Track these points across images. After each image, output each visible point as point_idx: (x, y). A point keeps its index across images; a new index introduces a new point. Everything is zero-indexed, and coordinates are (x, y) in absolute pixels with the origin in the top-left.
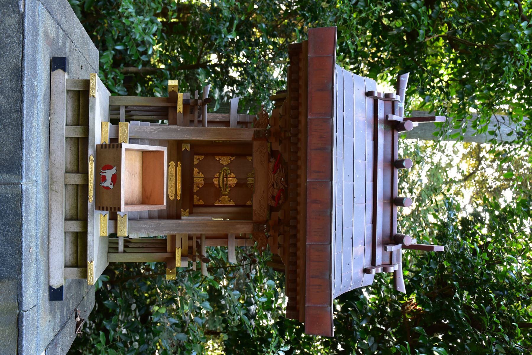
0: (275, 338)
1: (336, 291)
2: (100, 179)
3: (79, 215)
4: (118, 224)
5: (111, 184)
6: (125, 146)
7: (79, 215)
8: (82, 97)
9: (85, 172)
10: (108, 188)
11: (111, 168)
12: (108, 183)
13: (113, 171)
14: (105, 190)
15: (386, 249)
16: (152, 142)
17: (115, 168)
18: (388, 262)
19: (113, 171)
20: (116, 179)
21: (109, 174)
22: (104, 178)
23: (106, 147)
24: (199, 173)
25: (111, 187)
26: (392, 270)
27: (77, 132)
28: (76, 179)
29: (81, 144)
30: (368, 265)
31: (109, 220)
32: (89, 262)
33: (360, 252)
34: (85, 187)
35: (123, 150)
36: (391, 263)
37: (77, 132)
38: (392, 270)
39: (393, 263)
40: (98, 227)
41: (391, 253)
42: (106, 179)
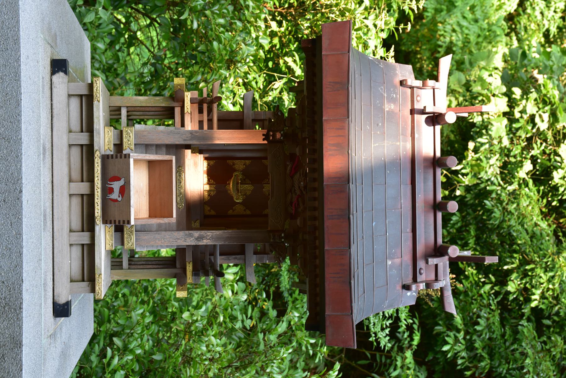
0: (307, 348)
1: (355, 323)
2: (107, 190)
3: (89, 225)
4: (125, 236)
5: (119, 197)
6: (134, 156)
7: (89, 225)
8: (88, 99)
9: (91, 180)
10: (116, 201)
11: (119, 179)
12: (115, 195)
13: (122, 182)
14: (112, 203)
15: (427, 262)
16: (158, 147)
17: (123, 179)
18: (433, 277)
19: (122, 182)
20: (125, 190)
21: (116, 186)
22: (111, 190)
23: (112, 157)
24: (209, 211)
25: (120, 199)
26: (438, 286)
27: (83, 139)
28: (84, 188)
29: (88, 150)
30: (409, 280)
31: (115, 232)
32: (97, 276)
33: (398, 262)
34: (91, 196)
35: (132, 161)
36: (437, 279)
37: (83, 139)
38: (438, 286)
39: (439, 279)
40: (104, 239)
41: (436, 266)
42: (113, 191)
